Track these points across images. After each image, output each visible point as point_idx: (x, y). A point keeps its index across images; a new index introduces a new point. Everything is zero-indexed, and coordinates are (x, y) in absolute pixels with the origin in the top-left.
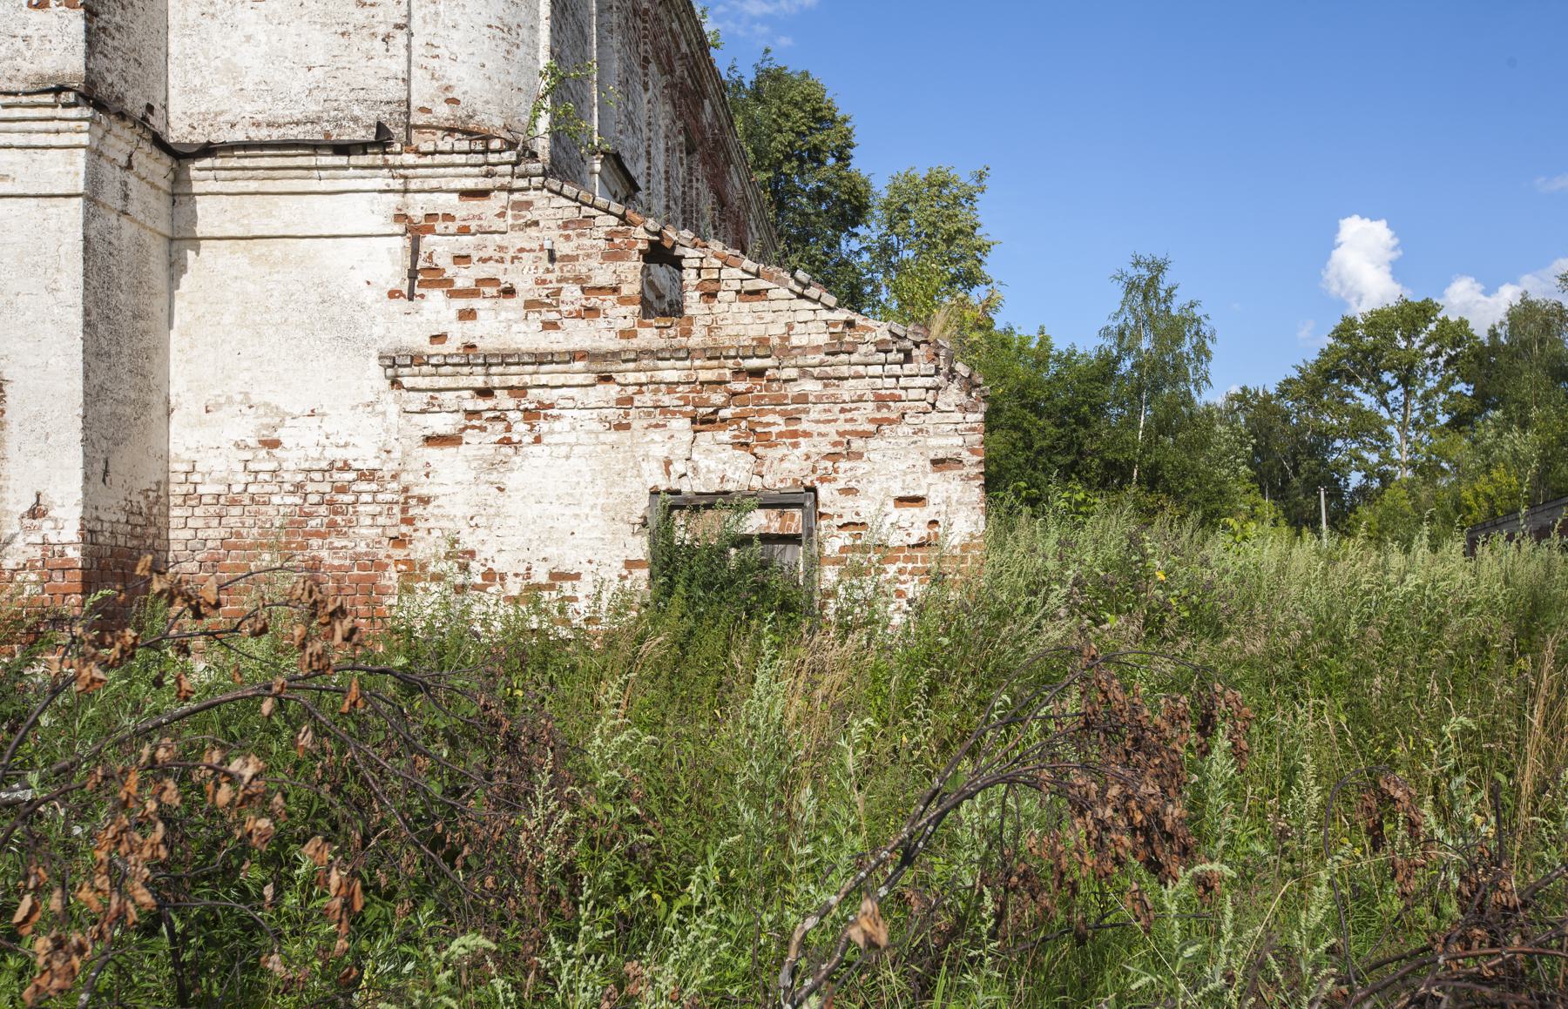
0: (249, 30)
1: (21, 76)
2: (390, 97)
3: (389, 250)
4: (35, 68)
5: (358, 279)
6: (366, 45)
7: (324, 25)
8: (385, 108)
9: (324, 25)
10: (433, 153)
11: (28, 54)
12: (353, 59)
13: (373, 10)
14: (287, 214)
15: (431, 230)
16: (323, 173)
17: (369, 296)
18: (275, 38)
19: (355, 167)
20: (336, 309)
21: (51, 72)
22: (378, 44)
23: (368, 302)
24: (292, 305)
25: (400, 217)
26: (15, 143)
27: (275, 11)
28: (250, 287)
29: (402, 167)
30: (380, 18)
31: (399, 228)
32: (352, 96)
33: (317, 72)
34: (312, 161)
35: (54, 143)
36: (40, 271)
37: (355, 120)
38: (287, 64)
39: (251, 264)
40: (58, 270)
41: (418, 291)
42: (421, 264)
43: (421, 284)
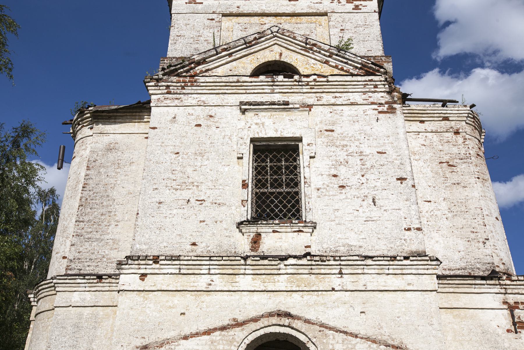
0: (437, 239)
1: (405, 251)
2: (489, 261)
3: (503, 314)
4: (409, 249)
5: (494, 324)
6: (477, 245)
7: (461, 238)
8: (488, 265)
9: (461, 238)
10: (516, 281)
11: (406, 245)
12: (474, 249)
13: (477, 234)
14: (464, 300)
15: (518, 308)
16: (476, 286)
17: (500, 331)
18: (446, 242)
19: (488, 285)
20: (489, 336)
21: (415, 250)
22: (481, 245)
23: (500, 333)
24: (472, 334)
25: (505, 303)
26: (414, 273)
27: (444, 234)
28: (455, 327)
29: (505, 285)
30: (480, 236)
31: (506, 307)
32: (476, 261)
33: (462, 253)
34: (473, 282)
35: (426, 273)
36: (426, 317)
37: (479, 269)
38: (451, 250)
39: (453, 318)
40: (432, 317)
41: (518, 330)
42: (516, 320)
43: (519, 327)
